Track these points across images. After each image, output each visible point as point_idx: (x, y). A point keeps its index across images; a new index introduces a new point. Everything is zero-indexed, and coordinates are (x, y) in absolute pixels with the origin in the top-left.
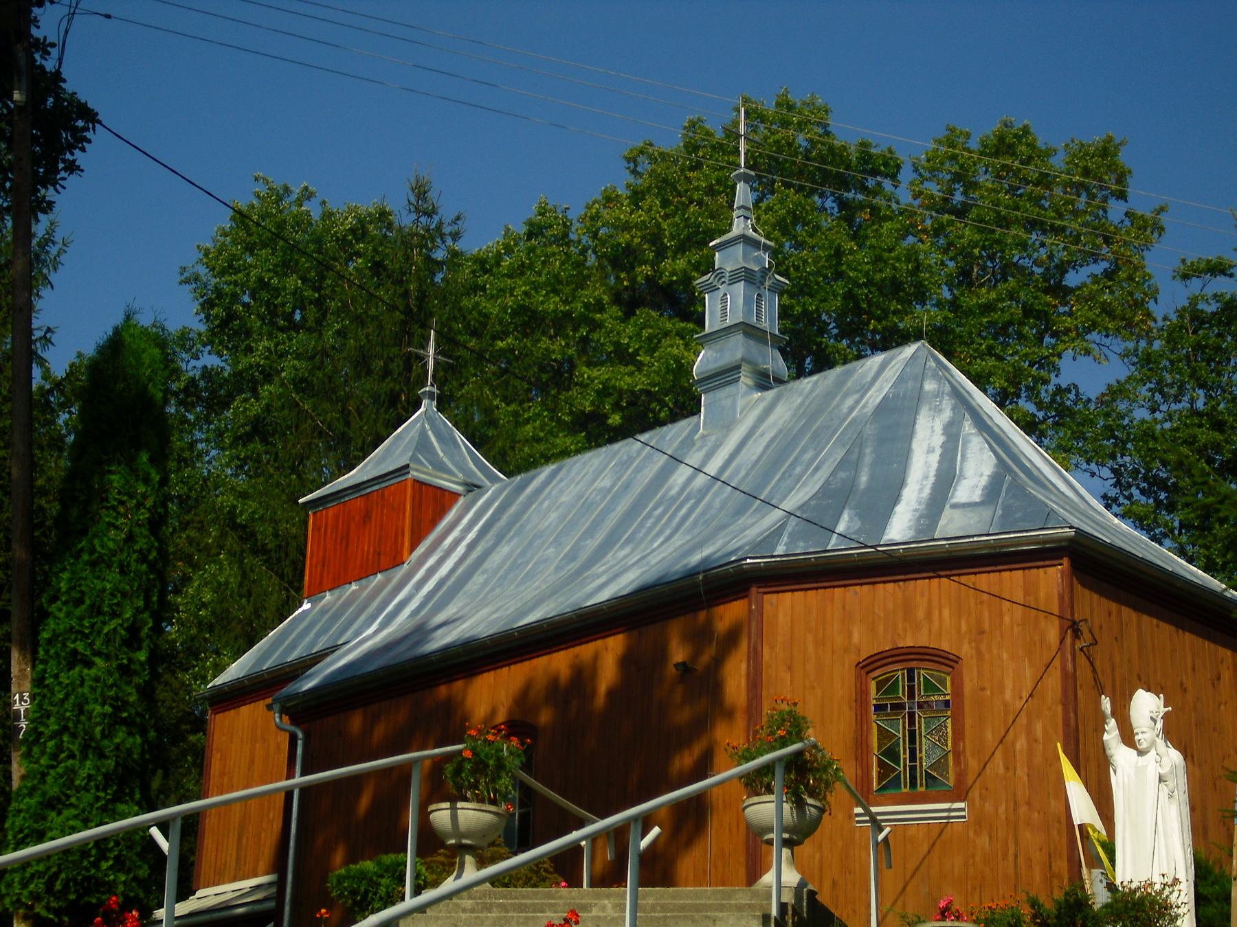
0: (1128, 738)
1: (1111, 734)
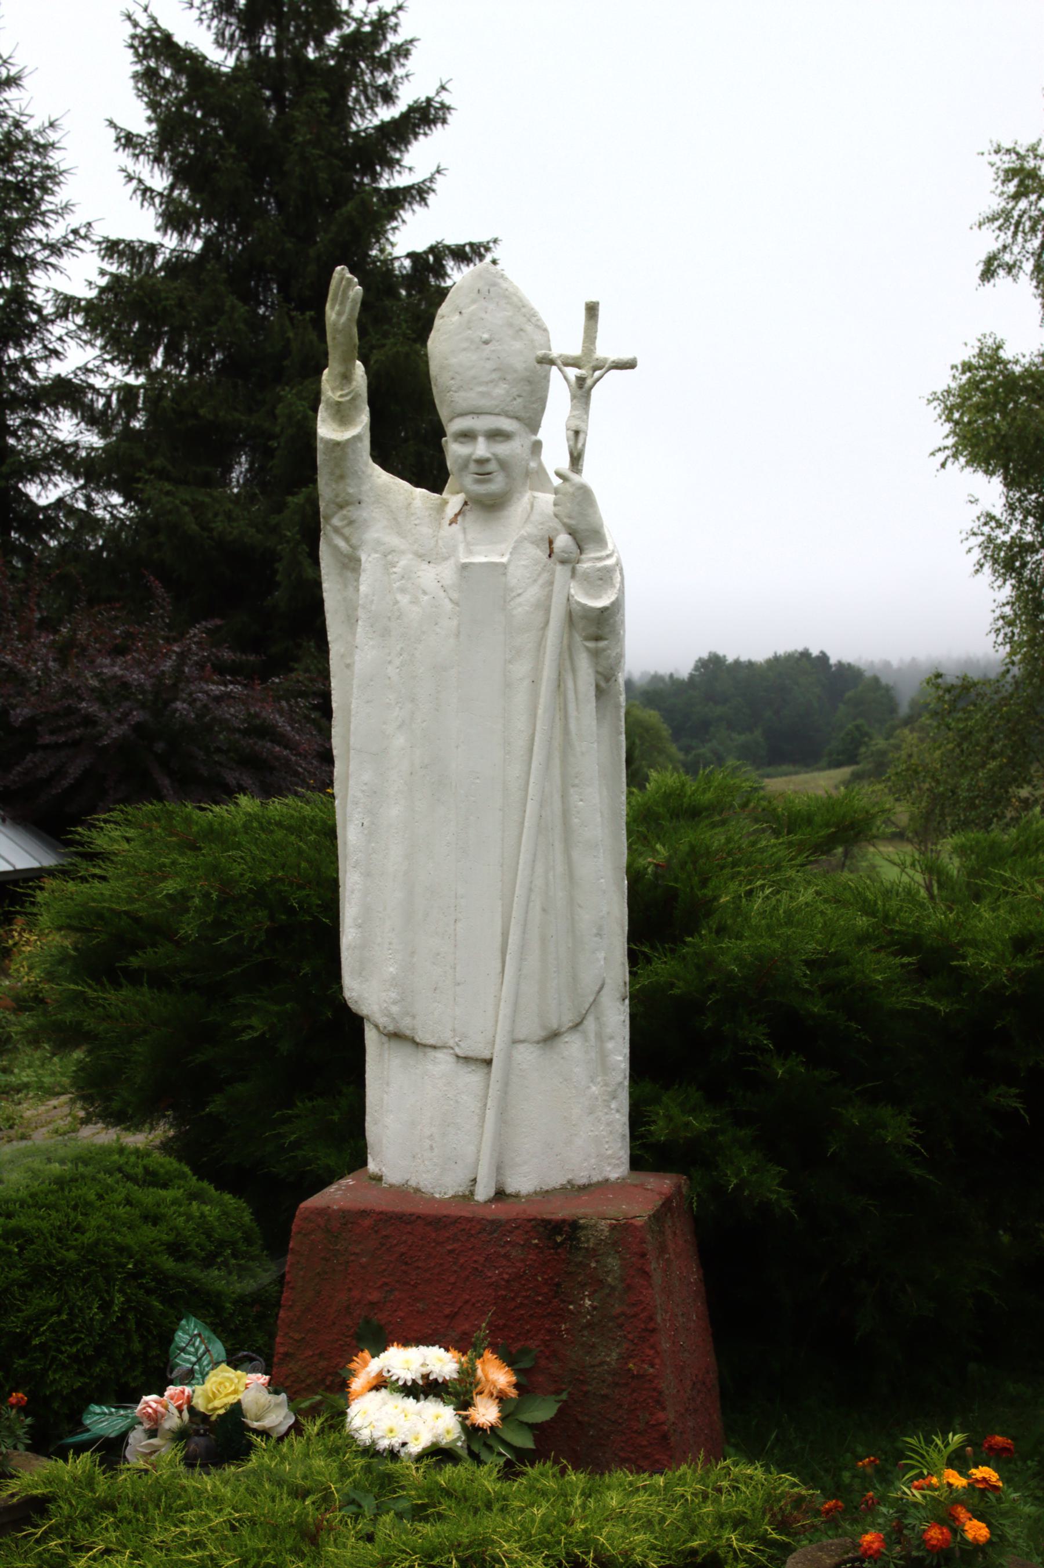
0: (412, 438)
1: (341, 426)
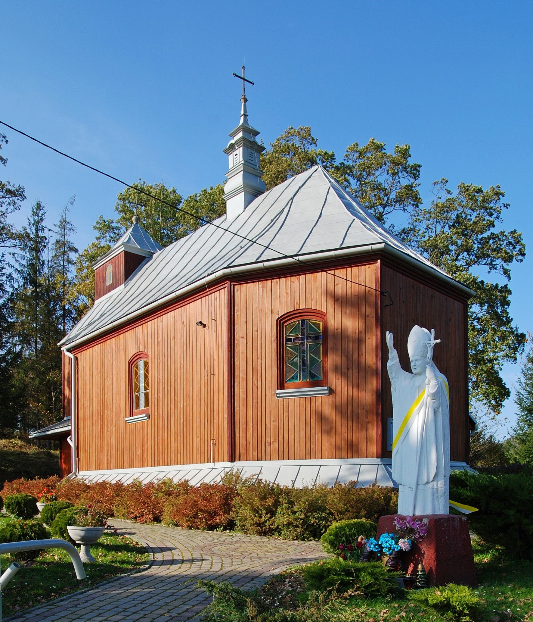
0: (405, 364)
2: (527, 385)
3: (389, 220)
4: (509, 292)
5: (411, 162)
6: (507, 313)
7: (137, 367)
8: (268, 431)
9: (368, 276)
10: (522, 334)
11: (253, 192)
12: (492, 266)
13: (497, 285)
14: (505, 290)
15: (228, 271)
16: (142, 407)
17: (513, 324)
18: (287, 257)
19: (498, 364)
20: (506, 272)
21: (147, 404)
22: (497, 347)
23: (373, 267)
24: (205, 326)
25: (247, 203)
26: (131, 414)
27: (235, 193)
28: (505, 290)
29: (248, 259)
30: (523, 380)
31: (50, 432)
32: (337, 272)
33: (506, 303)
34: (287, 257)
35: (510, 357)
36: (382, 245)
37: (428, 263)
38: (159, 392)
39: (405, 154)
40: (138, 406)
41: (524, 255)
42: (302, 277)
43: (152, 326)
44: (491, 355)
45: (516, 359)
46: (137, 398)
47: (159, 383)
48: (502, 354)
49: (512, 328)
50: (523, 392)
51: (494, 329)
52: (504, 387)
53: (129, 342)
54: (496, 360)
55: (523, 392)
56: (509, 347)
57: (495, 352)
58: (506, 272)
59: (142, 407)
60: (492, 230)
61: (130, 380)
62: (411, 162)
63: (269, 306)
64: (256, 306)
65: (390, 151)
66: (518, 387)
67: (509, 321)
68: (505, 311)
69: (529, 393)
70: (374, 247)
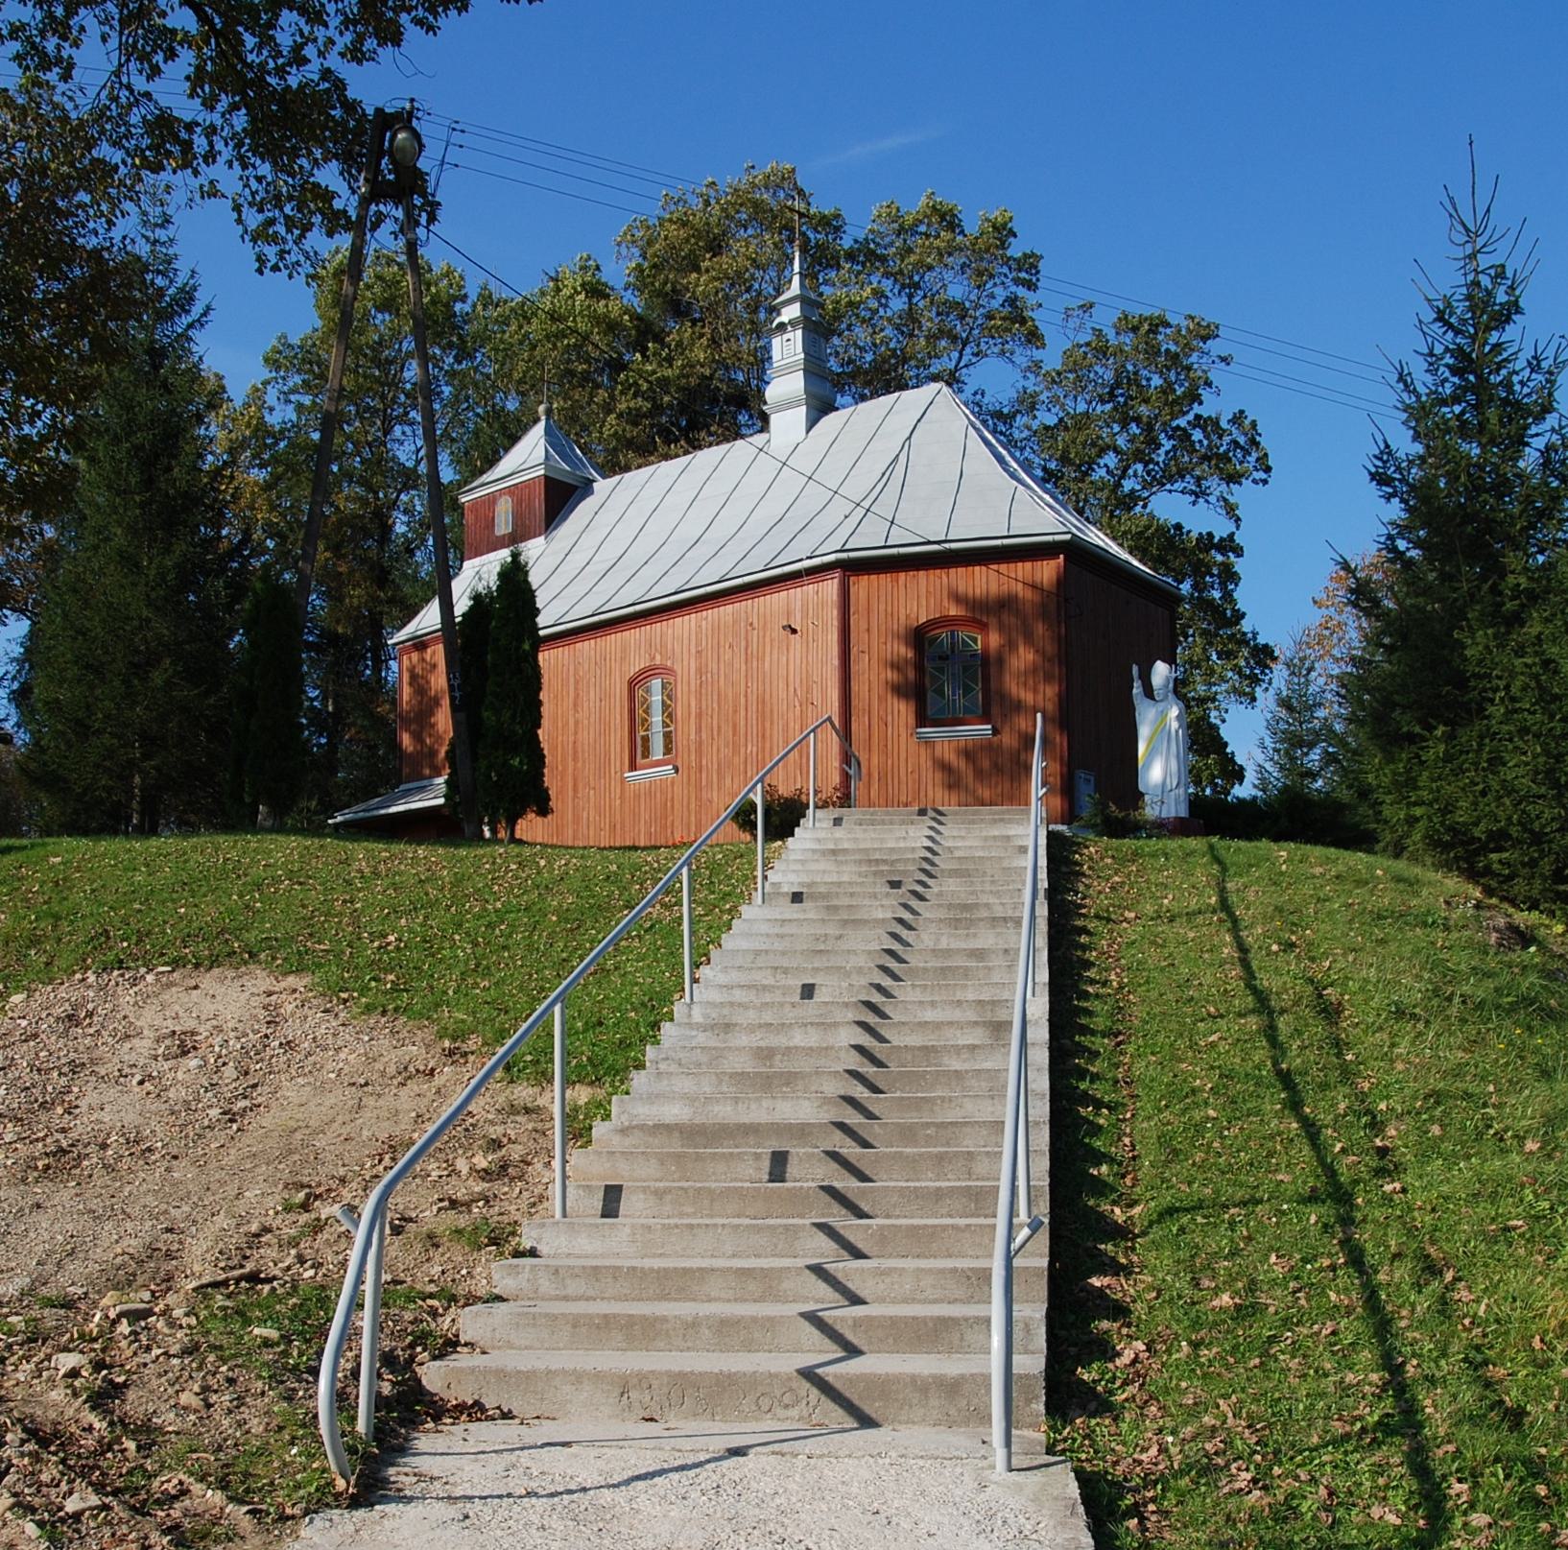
0: (1149, 692)
1: (1137, 689)
2: (1275, 750)
3: (973, 379)
4: (1239, 551)
5: (1016, 249)
6: (1233, 602)
7: (648, 691)
8: (903, 787)
9: (1047, 571)
10: (1266, 646)
11: (820, 407)
12: (1199, 494)
13: (1210, 535)
14: (1229, 545)
15: (844, 555)
16: (658, 754)
17: (1246, 626)
18: (929, 543)
19: (1217, 708)
20: (1230, 510)
21: (668, 750)
22: (1213, 672)
23: (1053, 563)
24: (794, 631)
25: (811, 423)
26: (633, 767)
27: (788, 405)
28: (1229, 545)
29: (870, 539)
30: (1268, 742)
31: (393, 810)
32: (1003, 568)
33: (1229, 576)
34: (929, 543)
35: (1241, 694)
36: (1068, 537)
37: (1125, 556)
38: (699, 730)
39: (1003, 232)
40: (646, 753)
41: (1268, 470)
42: (952, 571)
43: (683, 625)
44: (1201, 689)
45: (1254, 699)
46: (646, 740)
47: (699, 715)
48: (1224, 687)
49: (1244, 634)
50: (1268, 766)
51: (1204, 633)
52: (1230, 759)
53: (634, 647)
54: (1214, 700)
55: (1268, 766)
56: (1240, 673)
57: (1211, 684)
58: (1230, 510)
59: (658, 754)
60: (1197, 409)
61: (632, 712)
62: (1016, 249)
63: (902, 611)
64: (882, 607)
65: (972, 225)
66: (1260, 758)
67: (1240, 616)
68: (1228, 596)
69: (1282, 768)
70: (1057, 538)
